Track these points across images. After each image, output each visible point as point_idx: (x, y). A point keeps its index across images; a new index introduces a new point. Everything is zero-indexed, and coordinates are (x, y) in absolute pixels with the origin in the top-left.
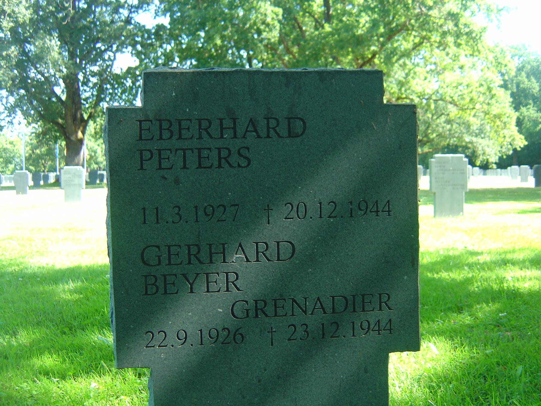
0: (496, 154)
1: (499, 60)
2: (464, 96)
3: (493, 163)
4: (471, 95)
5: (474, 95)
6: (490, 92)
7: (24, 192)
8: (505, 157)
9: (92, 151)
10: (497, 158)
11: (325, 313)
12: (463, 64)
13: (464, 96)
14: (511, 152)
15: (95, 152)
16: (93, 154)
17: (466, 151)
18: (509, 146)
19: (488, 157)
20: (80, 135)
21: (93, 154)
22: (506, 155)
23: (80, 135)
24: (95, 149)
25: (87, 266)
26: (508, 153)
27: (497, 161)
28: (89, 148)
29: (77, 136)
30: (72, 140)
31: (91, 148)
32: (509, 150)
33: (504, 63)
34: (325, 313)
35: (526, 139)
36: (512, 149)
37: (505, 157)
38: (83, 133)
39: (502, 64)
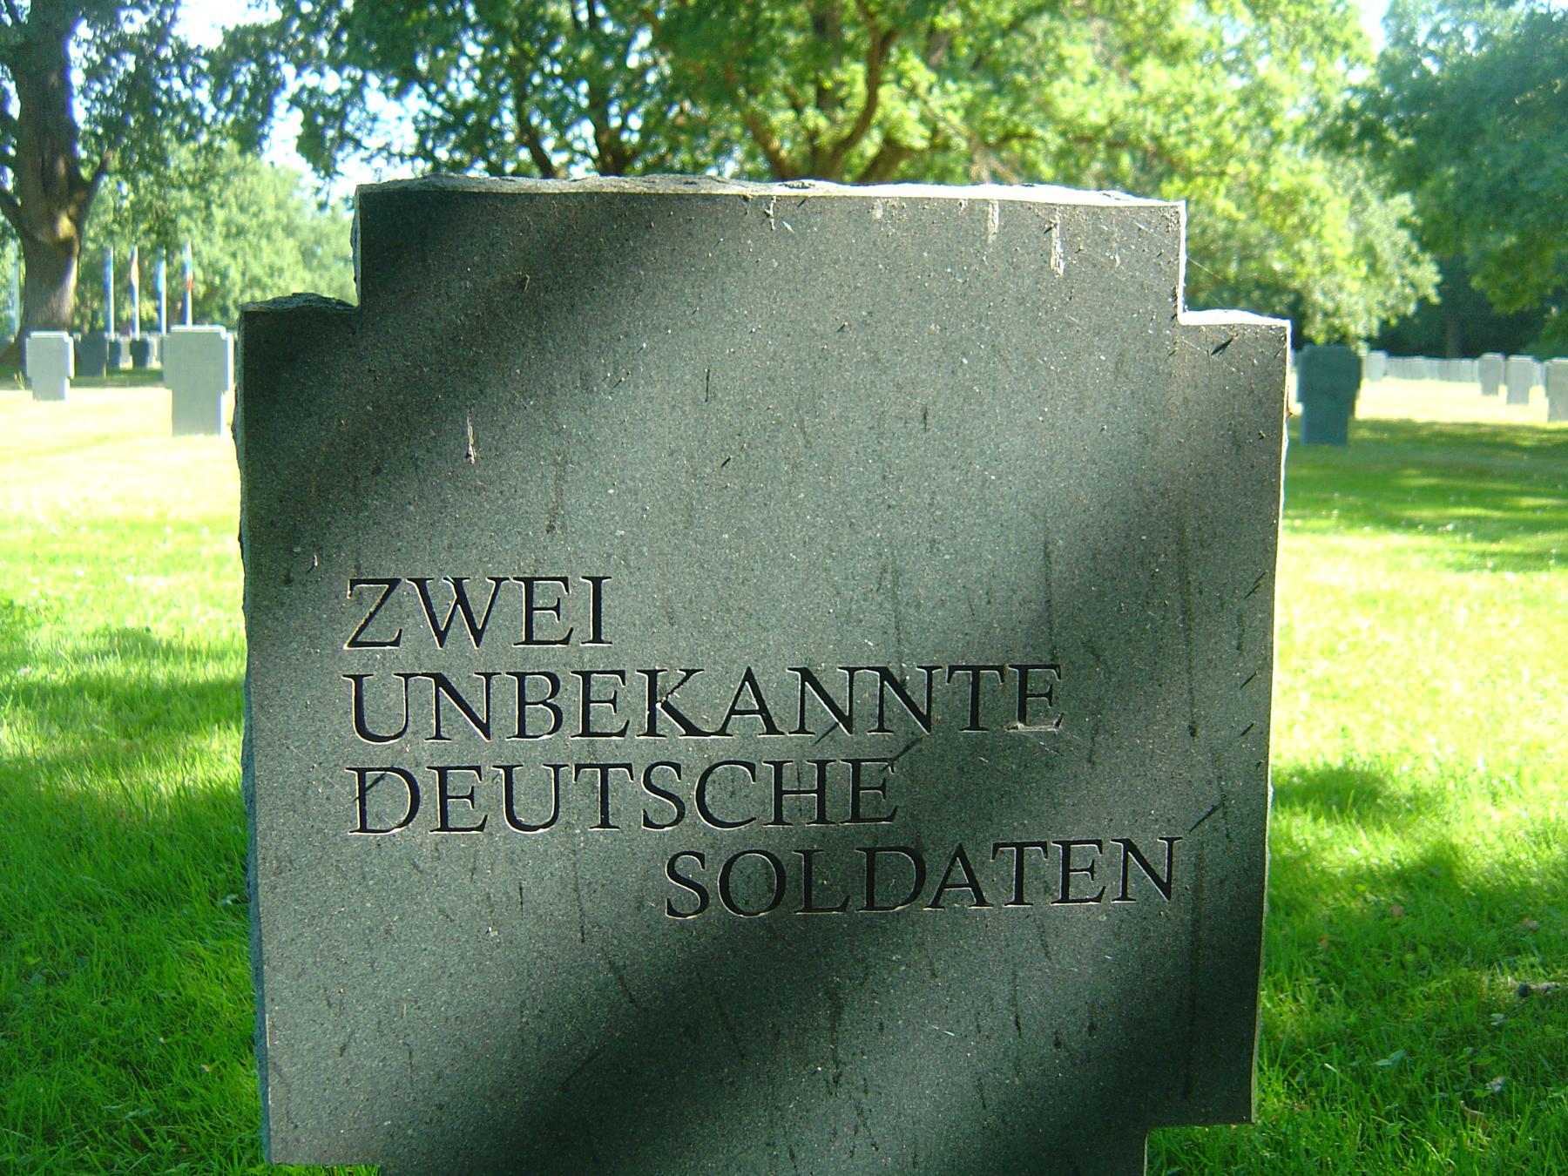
0: (1369, 311)
1: (1327, 30)
2: (1194, 135)
3: (1359, 338)
4: (1217, 132)
5: (1228, 133)
6: (1267, 123)
7: (59, 396)
8: (1394, 322)
9: (215, 272)
10: (1375, 324)
11: (771, 729)
12: (1184, 37)
13: (1194, 135)
14: (1411, 308)
15: (224, 276)
16: (217, 280)
17: (1275, 299)
18: (1408, 290)
19: (1346, 320)
20: (65, 226)
21: (217, 280)
22: (1397, 316)
23: (65, 226)
24: (222, 265)
25: (1302, 773)
26: (1402, 309)
27: (1375, 334)
28: (206, 262)
29: (54, 231)
30: (40, 243)
31: (210, 264)
32: (1405, 299)
33: (1341, 39)
34: (771, 729)
35: (1440, 272)
36: (1414, 298)
37: (1394, 322)
38: (78, 222)
39: (1334, 42)
